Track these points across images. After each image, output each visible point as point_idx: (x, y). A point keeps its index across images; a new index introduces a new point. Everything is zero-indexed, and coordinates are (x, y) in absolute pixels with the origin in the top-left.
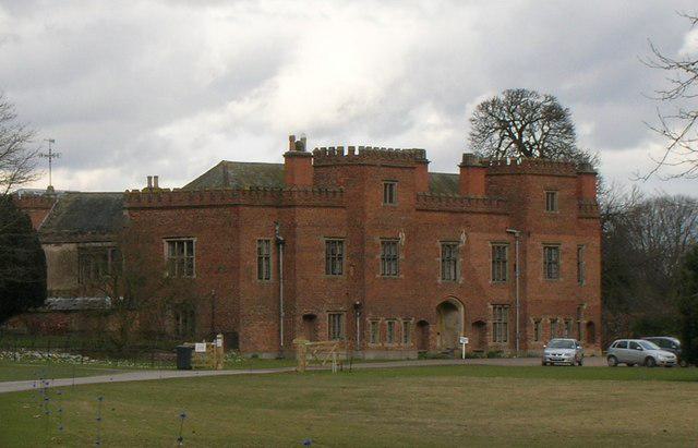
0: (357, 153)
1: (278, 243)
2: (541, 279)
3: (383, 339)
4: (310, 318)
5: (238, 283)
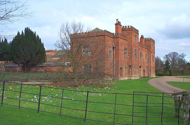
1: (113, 48)
3: (135, 74)
4: (121, 68)
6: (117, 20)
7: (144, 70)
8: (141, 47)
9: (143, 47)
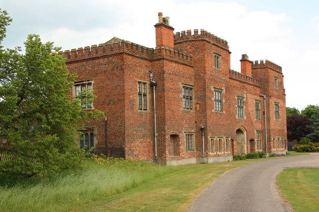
0: (199, 33)
1: (152, 85)
2: (274, 119)
3: (217, 150)
4: (174, 137)
5: (124, 111)
6: (160, 14)
7: (252, 141)
8: (241, 82)
9: (244, 83)
